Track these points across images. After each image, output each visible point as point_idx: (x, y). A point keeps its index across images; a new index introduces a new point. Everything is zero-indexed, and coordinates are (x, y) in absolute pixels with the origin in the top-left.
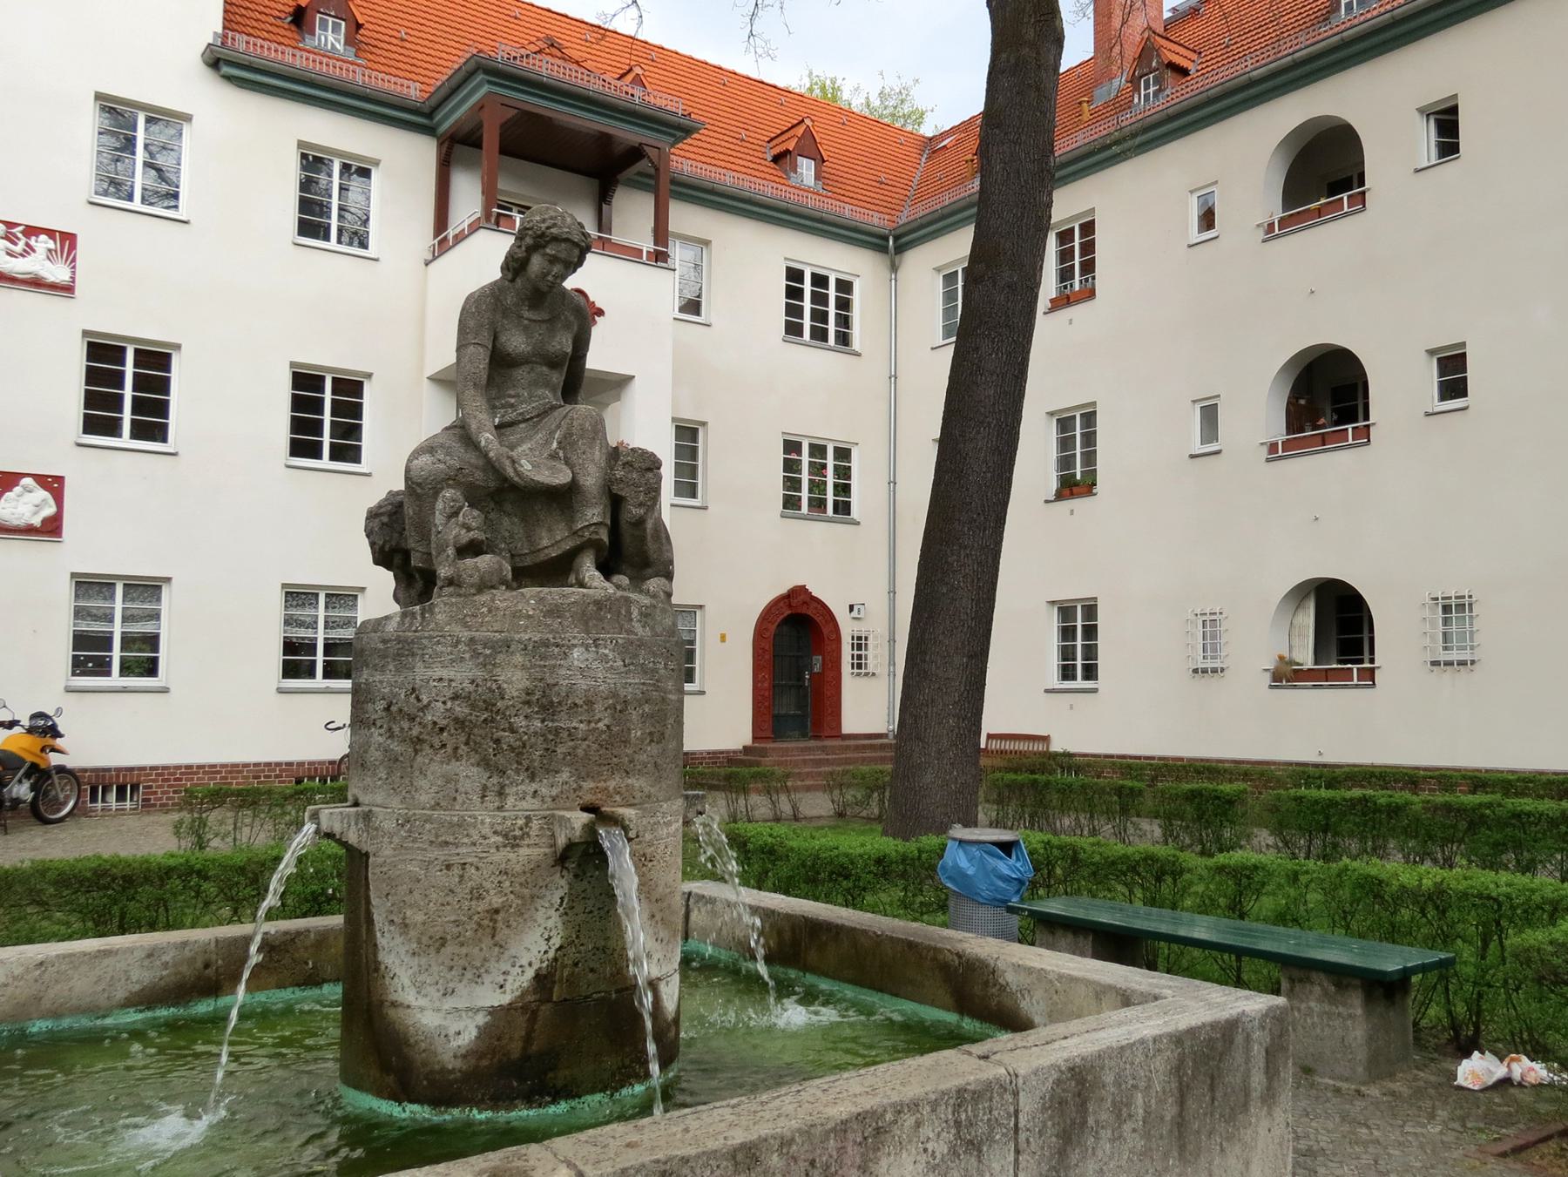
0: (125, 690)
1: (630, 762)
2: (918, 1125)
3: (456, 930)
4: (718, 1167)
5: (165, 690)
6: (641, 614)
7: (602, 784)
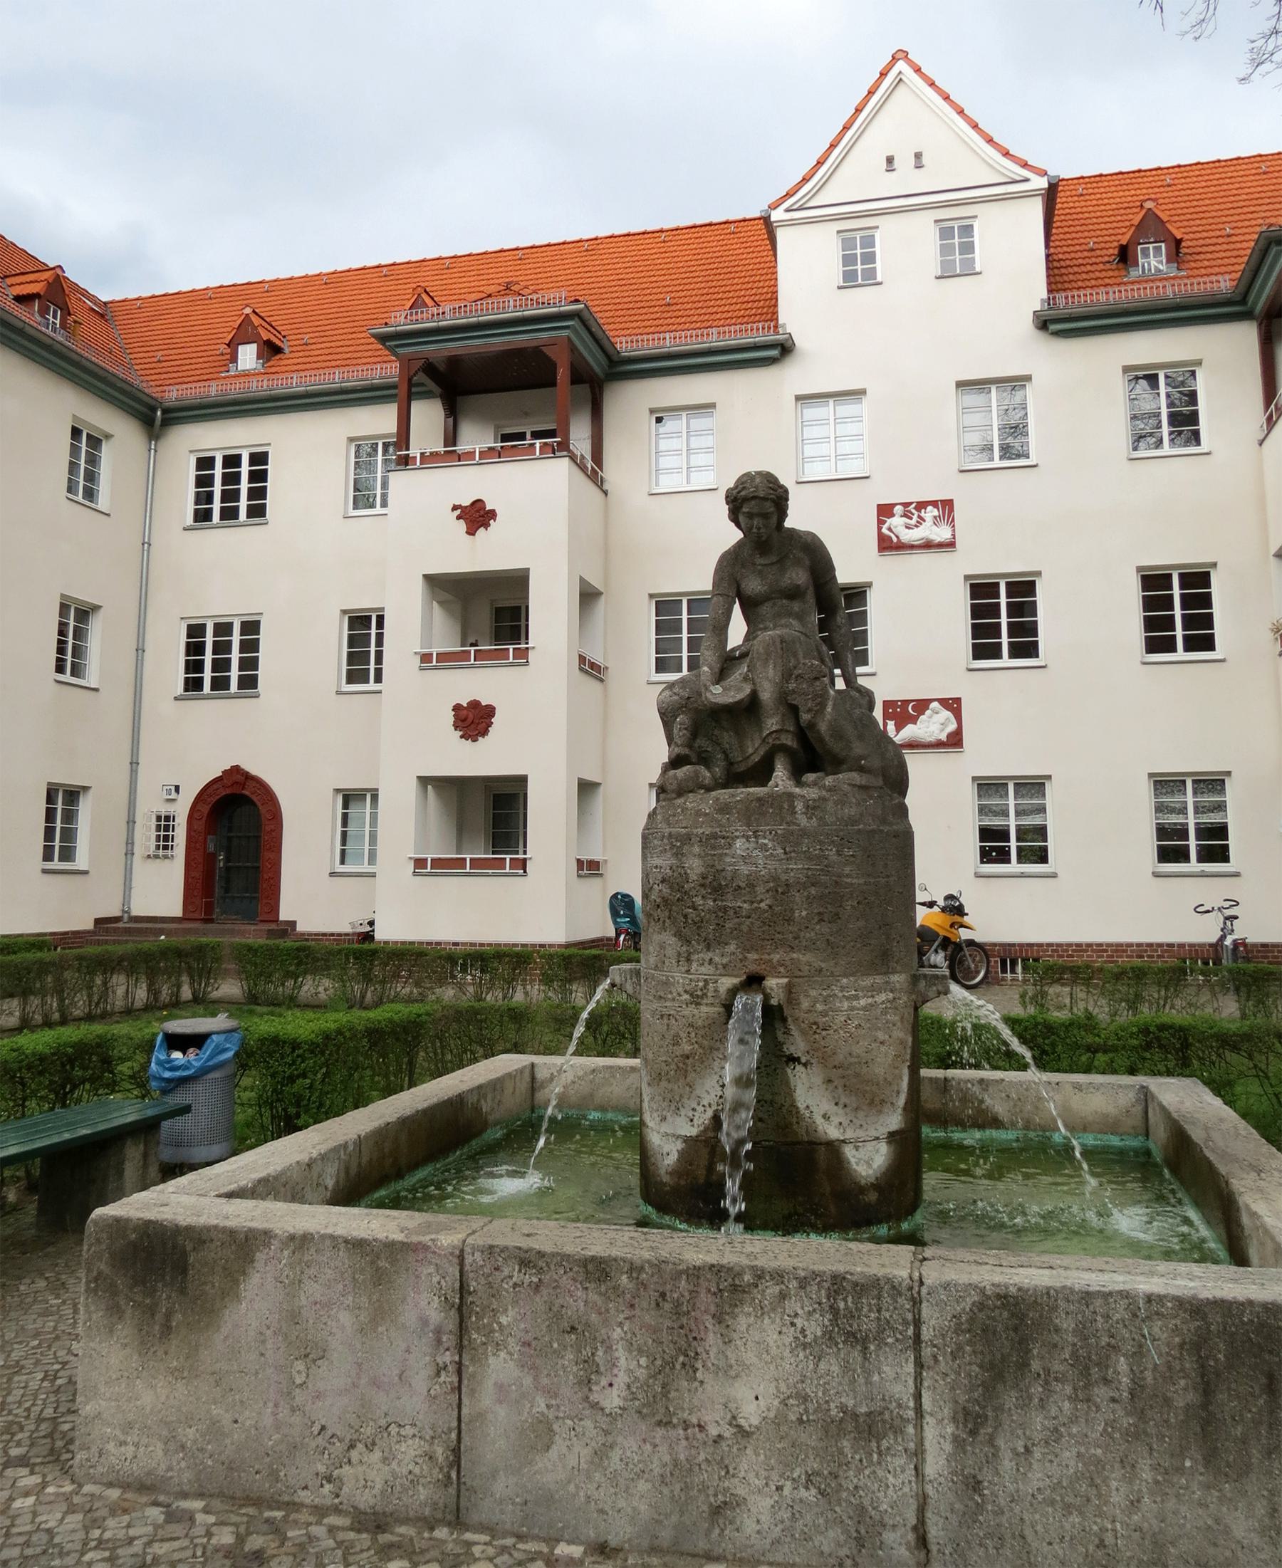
0: (1023, 876)
1: (795, 938)
2: (783, 1296)
4: (571, 1269)
5: (1054, 876)
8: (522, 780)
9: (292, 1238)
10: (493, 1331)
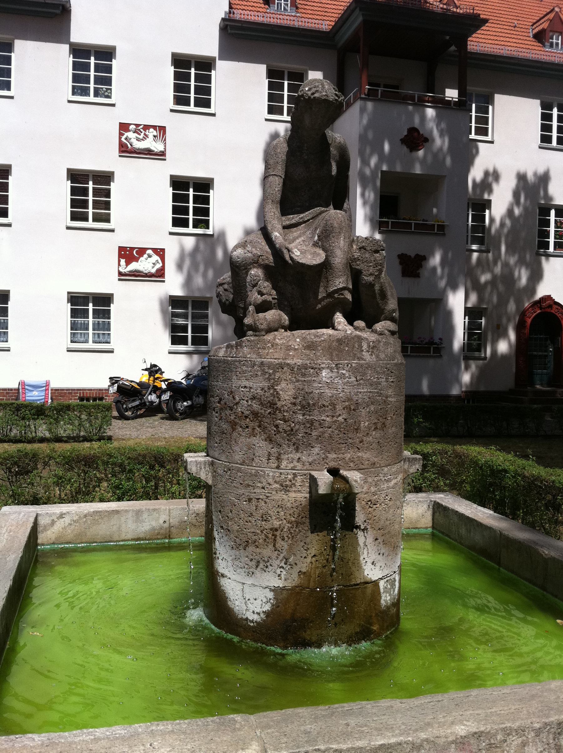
1: (361, 442)
3: (254, 538)
6: (369, 346)
7: (341, 456)
8: (112, 295)
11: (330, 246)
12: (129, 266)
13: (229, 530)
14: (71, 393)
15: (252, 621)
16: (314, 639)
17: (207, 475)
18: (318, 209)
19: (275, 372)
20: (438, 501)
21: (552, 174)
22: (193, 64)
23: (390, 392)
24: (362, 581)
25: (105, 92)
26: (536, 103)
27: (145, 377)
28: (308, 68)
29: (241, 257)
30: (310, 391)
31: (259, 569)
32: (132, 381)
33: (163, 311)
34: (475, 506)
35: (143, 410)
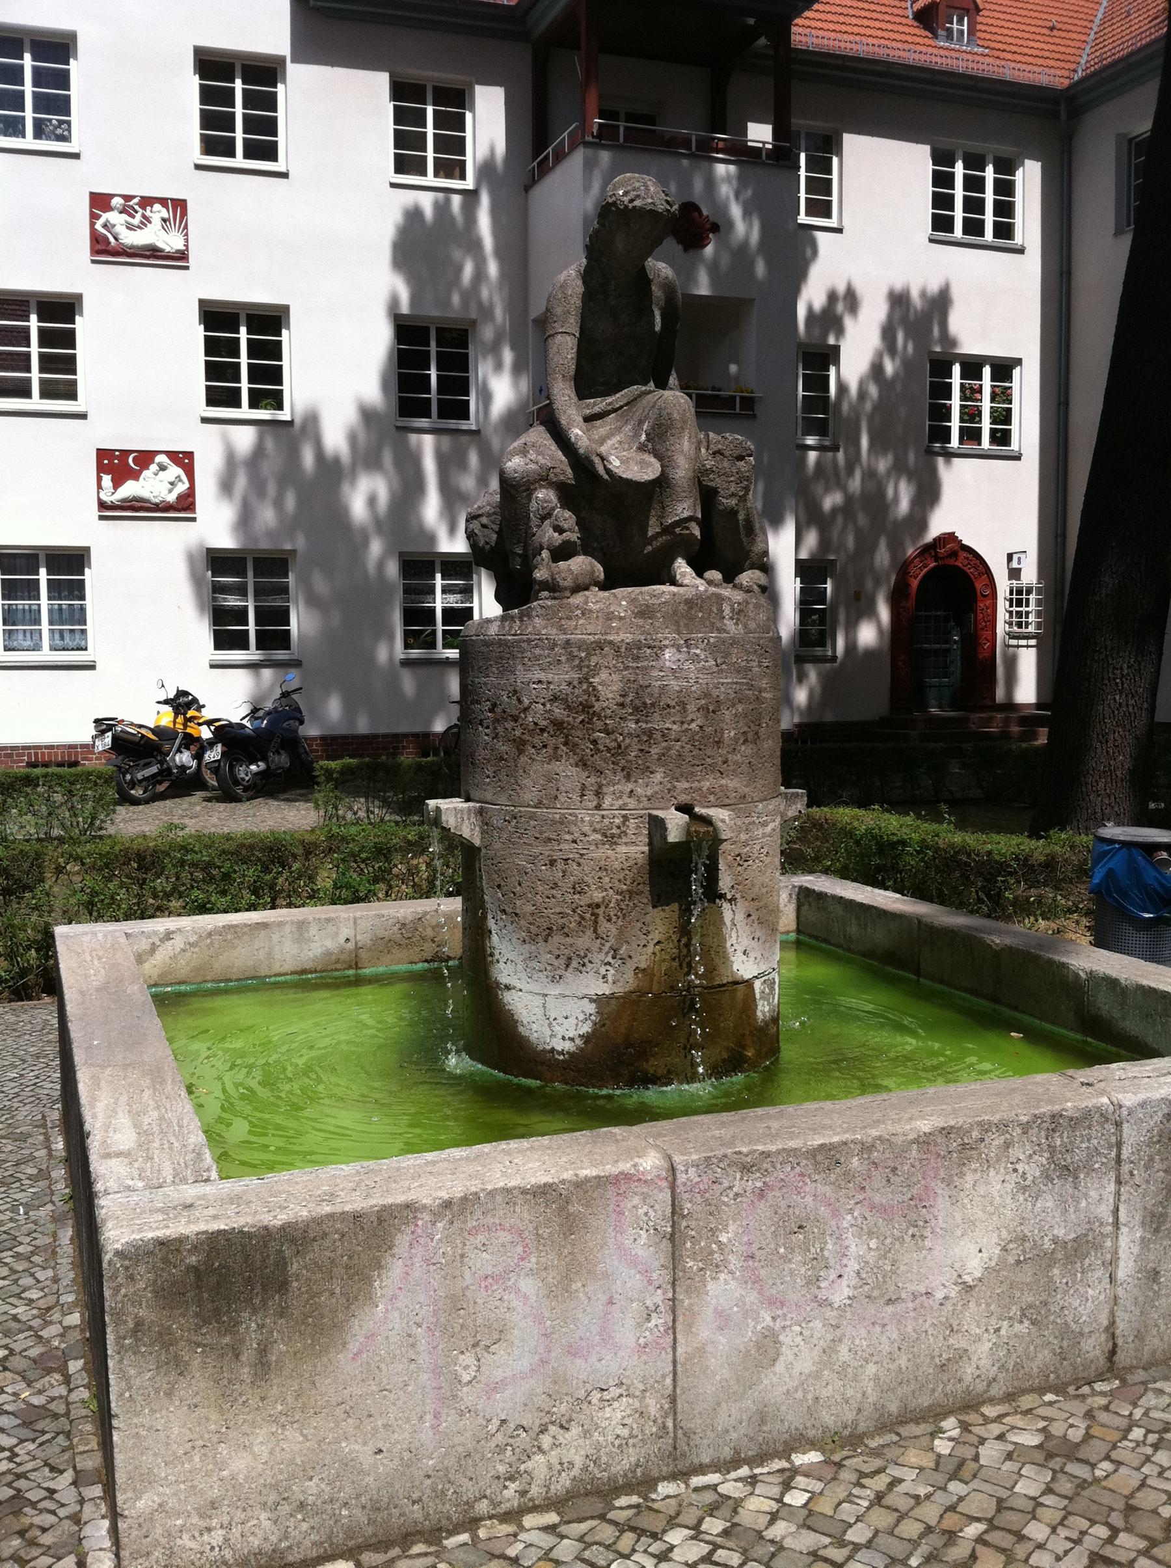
1: (725, 762)
2: (1008, 1145)
4: (798, 1164)
6: (733, 610)
8: (87, 549)
9: (447, 1204)
10: (712, 1253)
11: (667, 450)
12: (120, 490)
13: (516, 914)
14: (10, 756)
15: (562, 1053)
16: (661, 1071)
17: (472, 830)
18: (635, 389)
19: (589, 655)
20: (806, 885)
21: (956, 293)
22: (238, 70)
23: (764, 683)
24: (730, 980)
25: (56, 128)
26: (923, 152)
27: (166, 717)
28: (473, 79)
29: (520, 469)
30: (647, 683)
31: (570, 970)
32: (141, 726)
33: (196, 580)
34: (869, 888)
35: (166, 784)
